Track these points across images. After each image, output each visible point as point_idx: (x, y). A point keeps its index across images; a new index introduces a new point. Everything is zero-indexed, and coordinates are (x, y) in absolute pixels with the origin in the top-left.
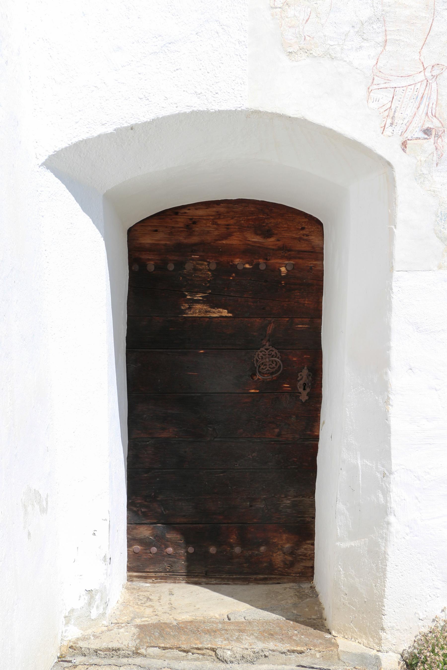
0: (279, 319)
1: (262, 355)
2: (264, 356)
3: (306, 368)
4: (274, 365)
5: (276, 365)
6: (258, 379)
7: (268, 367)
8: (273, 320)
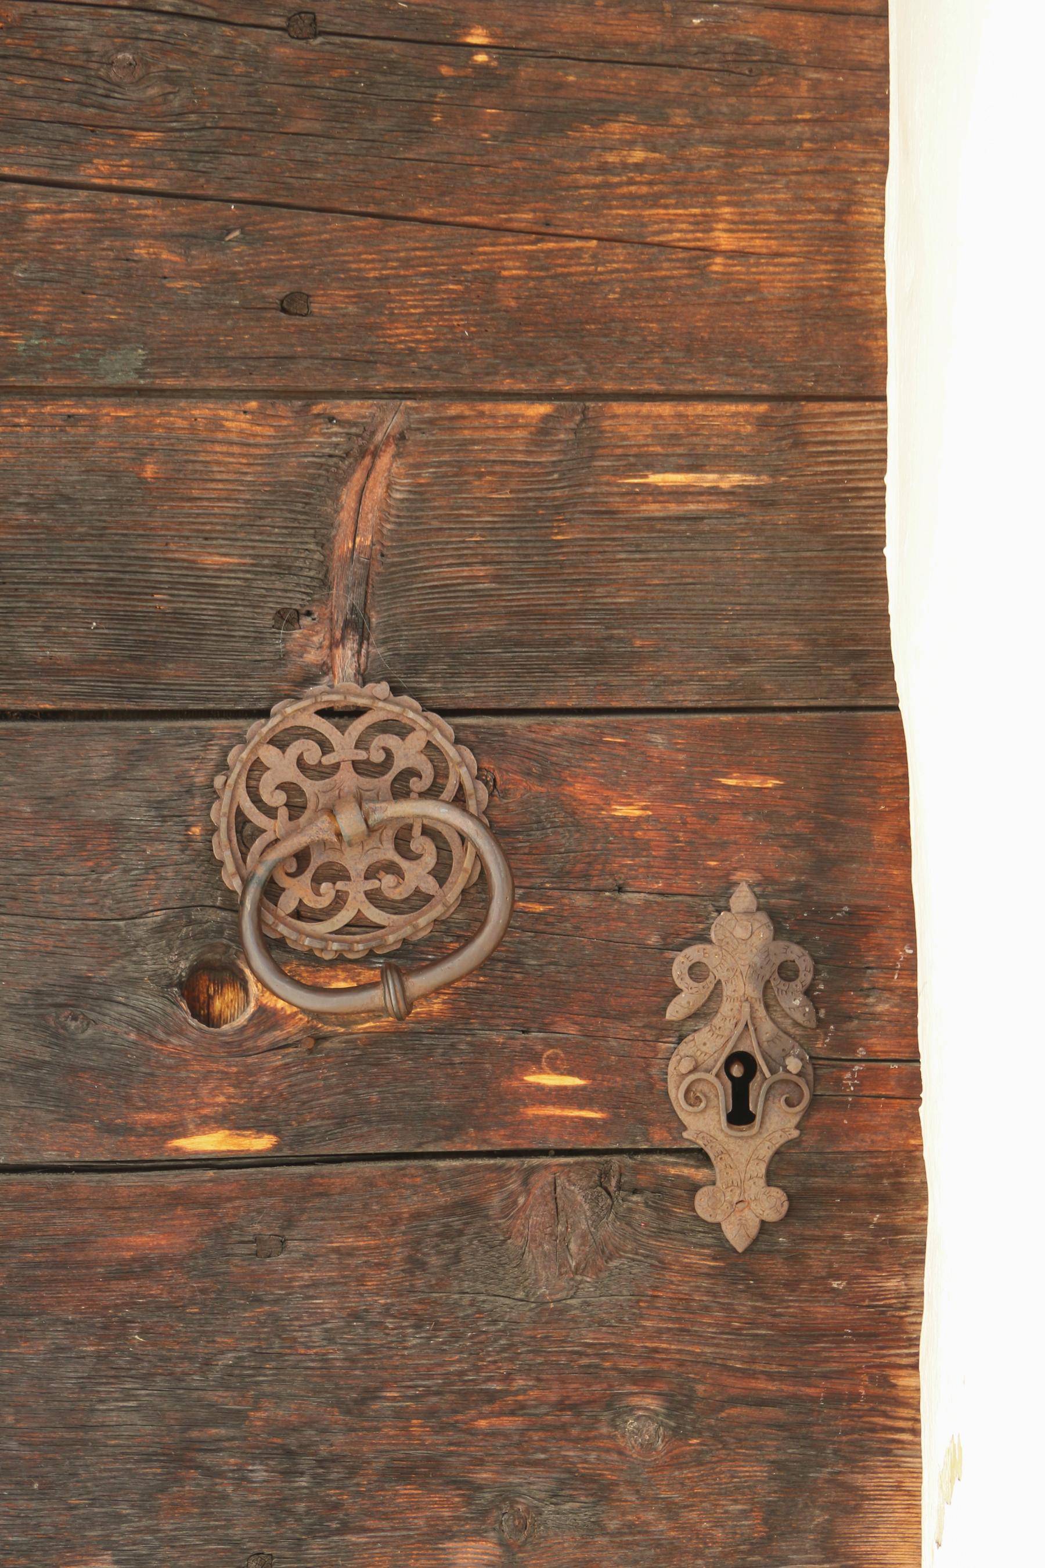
0: (455, 409)
1: (293, 775)
2: (308, 786)
3: (742, 898)
4: (418, 875)
5: (441, 873)
6: (266, 1018)
7: (356, 890)
8: (393, 423)
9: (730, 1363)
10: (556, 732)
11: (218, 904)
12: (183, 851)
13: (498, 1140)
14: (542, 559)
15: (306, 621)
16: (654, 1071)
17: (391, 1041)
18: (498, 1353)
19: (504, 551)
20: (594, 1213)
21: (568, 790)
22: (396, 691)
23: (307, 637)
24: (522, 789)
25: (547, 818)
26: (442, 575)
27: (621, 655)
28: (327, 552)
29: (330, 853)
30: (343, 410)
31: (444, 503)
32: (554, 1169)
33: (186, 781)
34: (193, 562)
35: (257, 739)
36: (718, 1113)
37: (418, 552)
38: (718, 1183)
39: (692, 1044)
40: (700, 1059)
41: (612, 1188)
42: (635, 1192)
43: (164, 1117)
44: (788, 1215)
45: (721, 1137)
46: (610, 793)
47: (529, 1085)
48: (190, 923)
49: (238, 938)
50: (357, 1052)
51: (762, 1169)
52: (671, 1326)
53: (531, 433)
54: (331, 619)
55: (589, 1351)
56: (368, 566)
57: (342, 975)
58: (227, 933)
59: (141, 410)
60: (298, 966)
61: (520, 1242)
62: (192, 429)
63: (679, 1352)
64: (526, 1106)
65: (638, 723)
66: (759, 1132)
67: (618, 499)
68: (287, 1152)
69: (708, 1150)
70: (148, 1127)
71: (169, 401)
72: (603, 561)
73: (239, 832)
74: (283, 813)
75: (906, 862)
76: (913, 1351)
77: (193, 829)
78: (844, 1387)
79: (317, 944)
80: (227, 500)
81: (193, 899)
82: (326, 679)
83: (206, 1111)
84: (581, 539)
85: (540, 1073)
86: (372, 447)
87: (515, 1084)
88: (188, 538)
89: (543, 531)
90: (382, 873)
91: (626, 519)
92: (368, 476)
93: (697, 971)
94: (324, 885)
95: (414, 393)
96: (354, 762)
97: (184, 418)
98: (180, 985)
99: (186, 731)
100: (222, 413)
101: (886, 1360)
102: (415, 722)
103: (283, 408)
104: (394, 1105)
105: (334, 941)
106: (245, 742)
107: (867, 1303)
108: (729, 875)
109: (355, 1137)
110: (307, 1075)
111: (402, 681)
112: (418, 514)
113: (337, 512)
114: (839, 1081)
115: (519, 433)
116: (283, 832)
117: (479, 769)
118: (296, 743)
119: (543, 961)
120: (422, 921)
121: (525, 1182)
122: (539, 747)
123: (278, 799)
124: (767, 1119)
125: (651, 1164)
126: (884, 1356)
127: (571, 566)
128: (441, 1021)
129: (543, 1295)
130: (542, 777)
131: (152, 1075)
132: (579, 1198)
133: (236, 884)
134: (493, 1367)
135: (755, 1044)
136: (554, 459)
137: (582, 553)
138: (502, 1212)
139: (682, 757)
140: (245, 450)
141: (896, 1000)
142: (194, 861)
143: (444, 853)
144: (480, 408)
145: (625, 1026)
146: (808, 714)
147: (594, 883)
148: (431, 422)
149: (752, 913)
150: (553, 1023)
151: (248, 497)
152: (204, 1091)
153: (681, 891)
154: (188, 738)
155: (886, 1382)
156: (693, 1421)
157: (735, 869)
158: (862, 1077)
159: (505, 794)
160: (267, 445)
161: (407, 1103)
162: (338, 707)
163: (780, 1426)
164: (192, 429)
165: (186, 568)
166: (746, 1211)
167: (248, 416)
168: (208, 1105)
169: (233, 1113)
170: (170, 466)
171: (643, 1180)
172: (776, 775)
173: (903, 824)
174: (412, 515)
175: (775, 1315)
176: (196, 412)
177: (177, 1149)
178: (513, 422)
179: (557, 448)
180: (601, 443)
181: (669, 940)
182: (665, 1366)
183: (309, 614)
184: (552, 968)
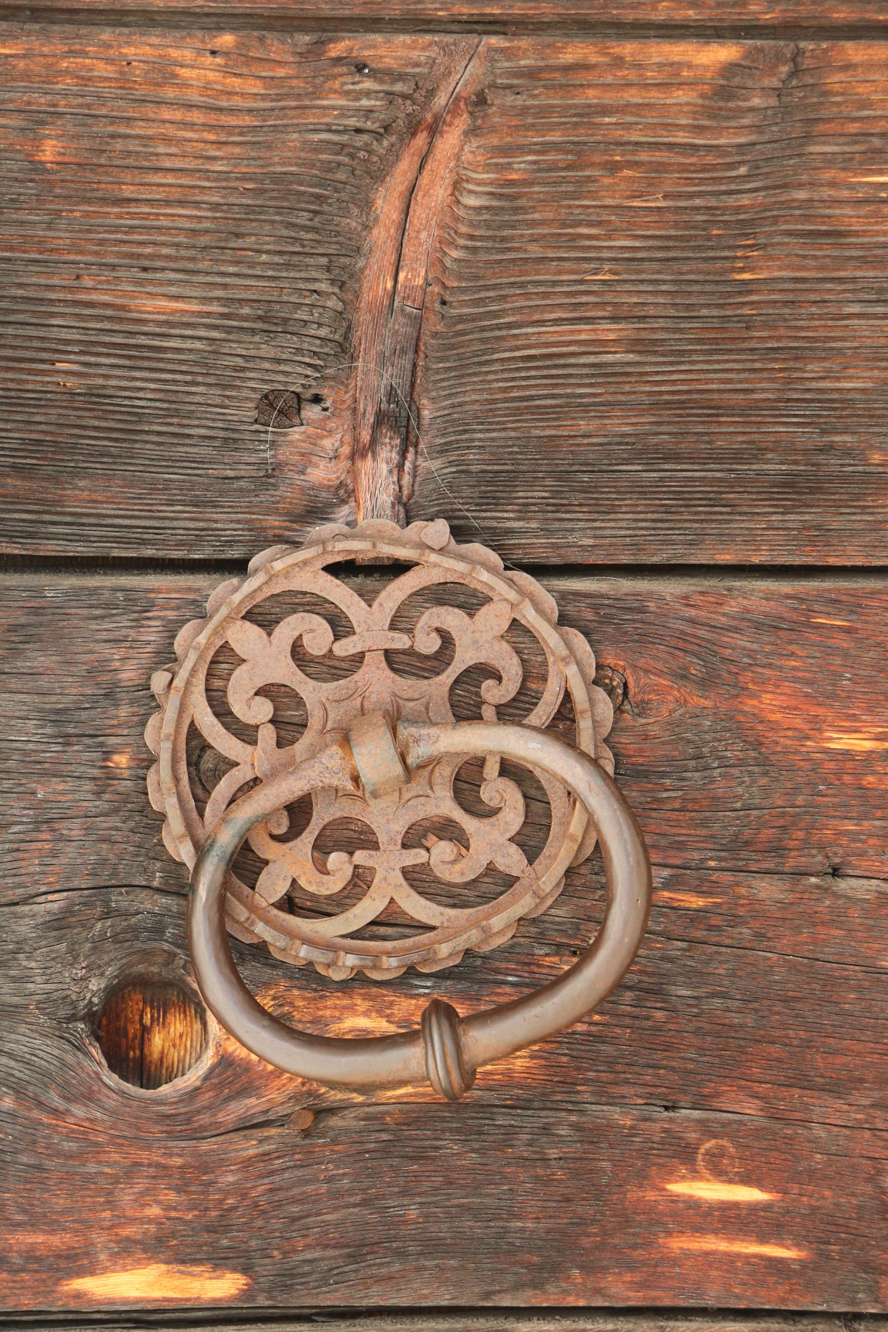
0: (574, 52)
1: (285, 672)
2: (312, 692)
4: (492, 842)
5: (531, 840)
6: (232, 1078)
7: (388, 865)
8: (466, 75)
10: (733, 607)
11: (156, 883)
12: (98, 794)
13: (621, 1290)
14: (715, 313)
15: (311, 412)
17: (443, 1119)
19: (651, 299)
21: (750, 705)
22: (461, 533)
23: (313, 440)
24: (671, 703)
25: (714, 750)
26: (543, 339)
27: (845, 479)
28: (349, 297)
29: (345, 802)
30: (381, 52)
31: (551, 215)
33: (106, 677)
34: (122, 308)
35: (224, 611)
37: (504, 298)
43: (56, 1240)
46: (821, 711)
47: (674, 1199)
48: (107, 914)
49: (185, 942)
50: (385, 1136)
53: (702, 96)
54: (355, 410)
56: (418, 322)
57: (362, 1005)
58: (170, 932)
59: (36, 44)
60: (289, 989)
62: (123, 81)
64: (669, 1234)
65: (873, 593)
67: (848, 211)
68: (262, 1301)
70: (31, 1256)
71: (84, 30)
72: (820, 317)
73: (193, 763)
74: (267, 734)
77: (116, 758)
79: (317, 956)
80: (182, 203)
81: (114, 874)
82: (345, 510)
83: (128, 1231)
84: (784, 280)
85: (694, 1179)
86: (429, 117)
87: (651, 1196)
88: (113, 267)
89: (719, 264)
90: (432, 838)
91: (862, 246)
92: (421, 167)
94: (333, 856)
95: (505, 23)
96: (387, 653)
97: (110, 61)
98: (90, 1017)
99: (107, 594)
100: (174, 53)
102: (492, 588)
103: (280, 48)
104: (445, 1227)
105: (348, 951)
106: (204, 616)
109: (379, 1280)
110: (299, 1173)
111: (474, 518)
112: (505, 233)
113: (366, 227)
115: (682, 96)
116: (266, 767)
117: (599, 667)
118: (291, 619)
120: (497, 922)
122: (702, 633)
123: (259, 712)
127: (765, 326)
128: (529, 1087)
130: (706, 683)
131: (39, 1168)
133: (185, 853)
136: (742, 140)
137: (785, 303)
140: (212, 118)
142: (116, 811)
143: (536, 807)
144: (617, 50)
145: (839, 1104)
147: (791, 863)
148: (532, 74)
150: (717, 1095)
151: (216, 199)
152: (126, 1197)
154: (108, 606)
159: (643, 708)
160: (250, 111)
161: (467, 1223)
162: (361, 559)
164: (123, 81)
165: (110, 319)
167: (219, 60)
168: (133, 1220)
169: (173, 1234)
170: (86, 143)
174: (495, 234)
176: (129, 51)
177: (79, 1295)
178: (673, 77)
179: (746, 121)
180: (824, 113)
183: (317, 399)
184: (717, 1002)
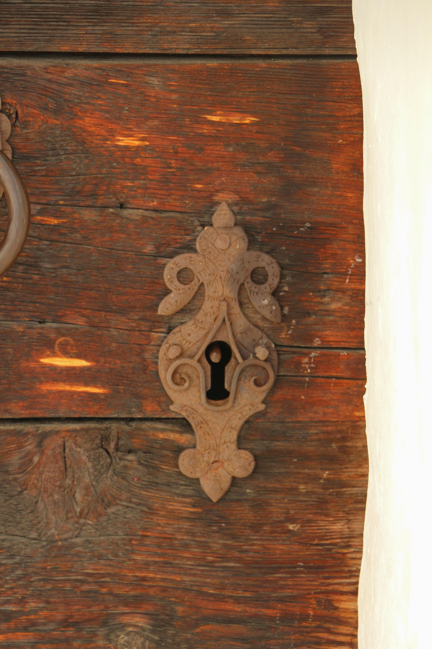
3: (223, 215)
9: (205, 589)
10: (69, 74)
16: (147, 356)
18: (15, 581)
20: (96, 469)
32: (63, 434)
36: (199, 391)
38: (198, 447)
39: (179, 334)
40: (186, 347)
41: (111, 450)
42: (130, 452)
44: (255, 471)
45: (201, 410)
46: (114, 126)
47: (44, 366)
51: (234, 435)
52: (157, 559)
55: (90, 579)
61: (34, 493)
63: (163, 580)
64: (41, 383)
66: (233, 407)
69: (190, 420)
75: (359, 188)
76: (353, 580)
78: (296, 608)
87: (32, 365)
93: (184, 276)
101: (331, 588)
107: (316, 542)
108: (211, 195)
114: (298, 365)
119: (57, 265)
121: (40, 445)
122: (54, 86)
124: (239, 396)
125: (143, 430)
126: (329, 585)
129: (53, 535)
130: (57, 112)
132: (84, 458)
134: (10, 592)
135: (230, 335)
138: (20, 468)
139: (174, 97)
141: (347, 299)
145: (124, 319)
146: (280, 61)
147: (100, 201)
149: (230, 228)
150: (64, 316)
153: (172, 208)
155: (330, 605)
156: (174, 635)
157: (217, 191)
158: (317, 362)
163: (244, 640)
166: (220, 470)
171: (136, 443)
172: (253, 114)
173: (357, 154)
175: (242, 551)
181: (162, 249)
182: (151, 592)
184: (65, 271)
